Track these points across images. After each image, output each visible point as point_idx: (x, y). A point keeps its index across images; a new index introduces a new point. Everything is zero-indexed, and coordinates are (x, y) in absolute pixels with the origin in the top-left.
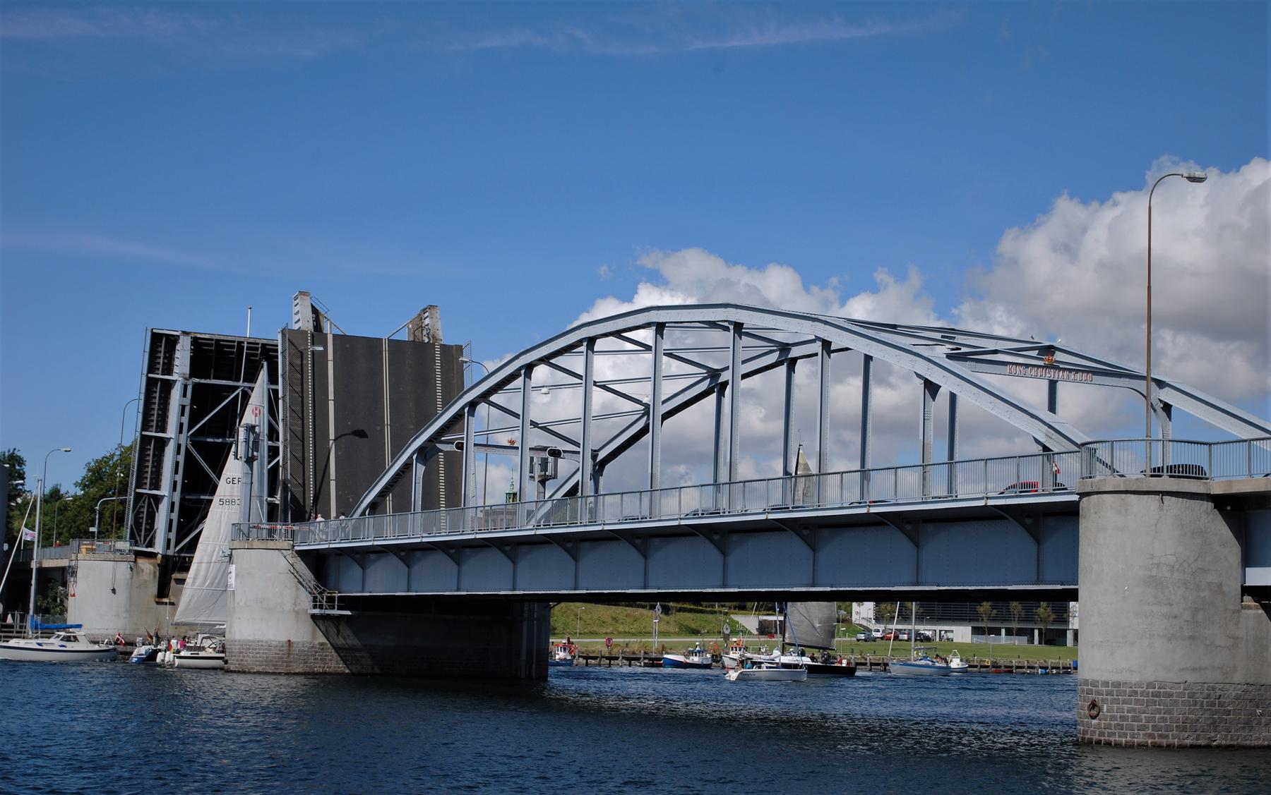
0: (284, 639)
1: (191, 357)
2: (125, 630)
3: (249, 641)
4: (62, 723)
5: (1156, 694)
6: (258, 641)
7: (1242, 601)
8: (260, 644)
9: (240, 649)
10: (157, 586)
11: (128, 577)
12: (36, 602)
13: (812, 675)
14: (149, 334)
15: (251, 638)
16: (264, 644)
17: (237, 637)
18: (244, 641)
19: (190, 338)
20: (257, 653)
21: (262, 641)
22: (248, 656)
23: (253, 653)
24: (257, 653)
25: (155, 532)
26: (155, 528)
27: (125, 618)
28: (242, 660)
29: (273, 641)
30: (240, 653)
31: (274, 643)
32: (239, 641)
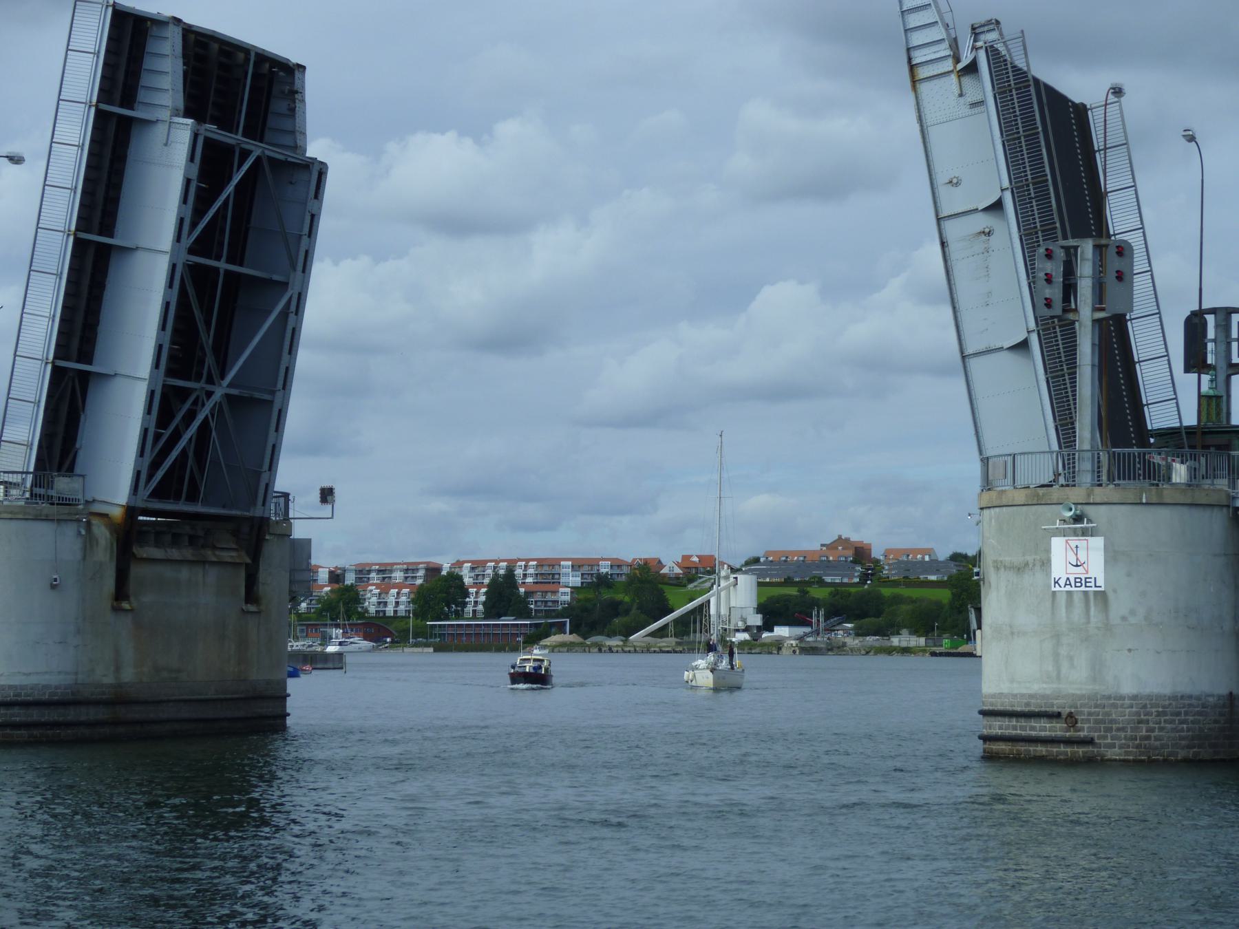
0: (1224, 691)
1: (185, 74)
2: (76, 673)
3: (1159, 697)
4: (799, 911)
5: (1144, 705)
6: (1182, 697)
7: (729, 566)
8: (1187, 702)
9: (1138, 714)
10: (114, 575)
11: (79, 556)
12: (453, 620)
13: (258, 697)
14: (110, 10)
15: (1167, 691)
16: (1194, 702)
17: (1128, 688)
18: (1149, 697)
19: (180, 29)
20: (1181, 722)
21: (1190, 697)
22: (1161, 729)
23: (1171, 722)
24: (1181, 722)
25: (76, 452)
26: (77, 446)
27: (76, 647)
28: (1148, 738)
29: (1209, 696)
30: (1140, 722)
31: (1211, 699)
32: (1135, 697)
